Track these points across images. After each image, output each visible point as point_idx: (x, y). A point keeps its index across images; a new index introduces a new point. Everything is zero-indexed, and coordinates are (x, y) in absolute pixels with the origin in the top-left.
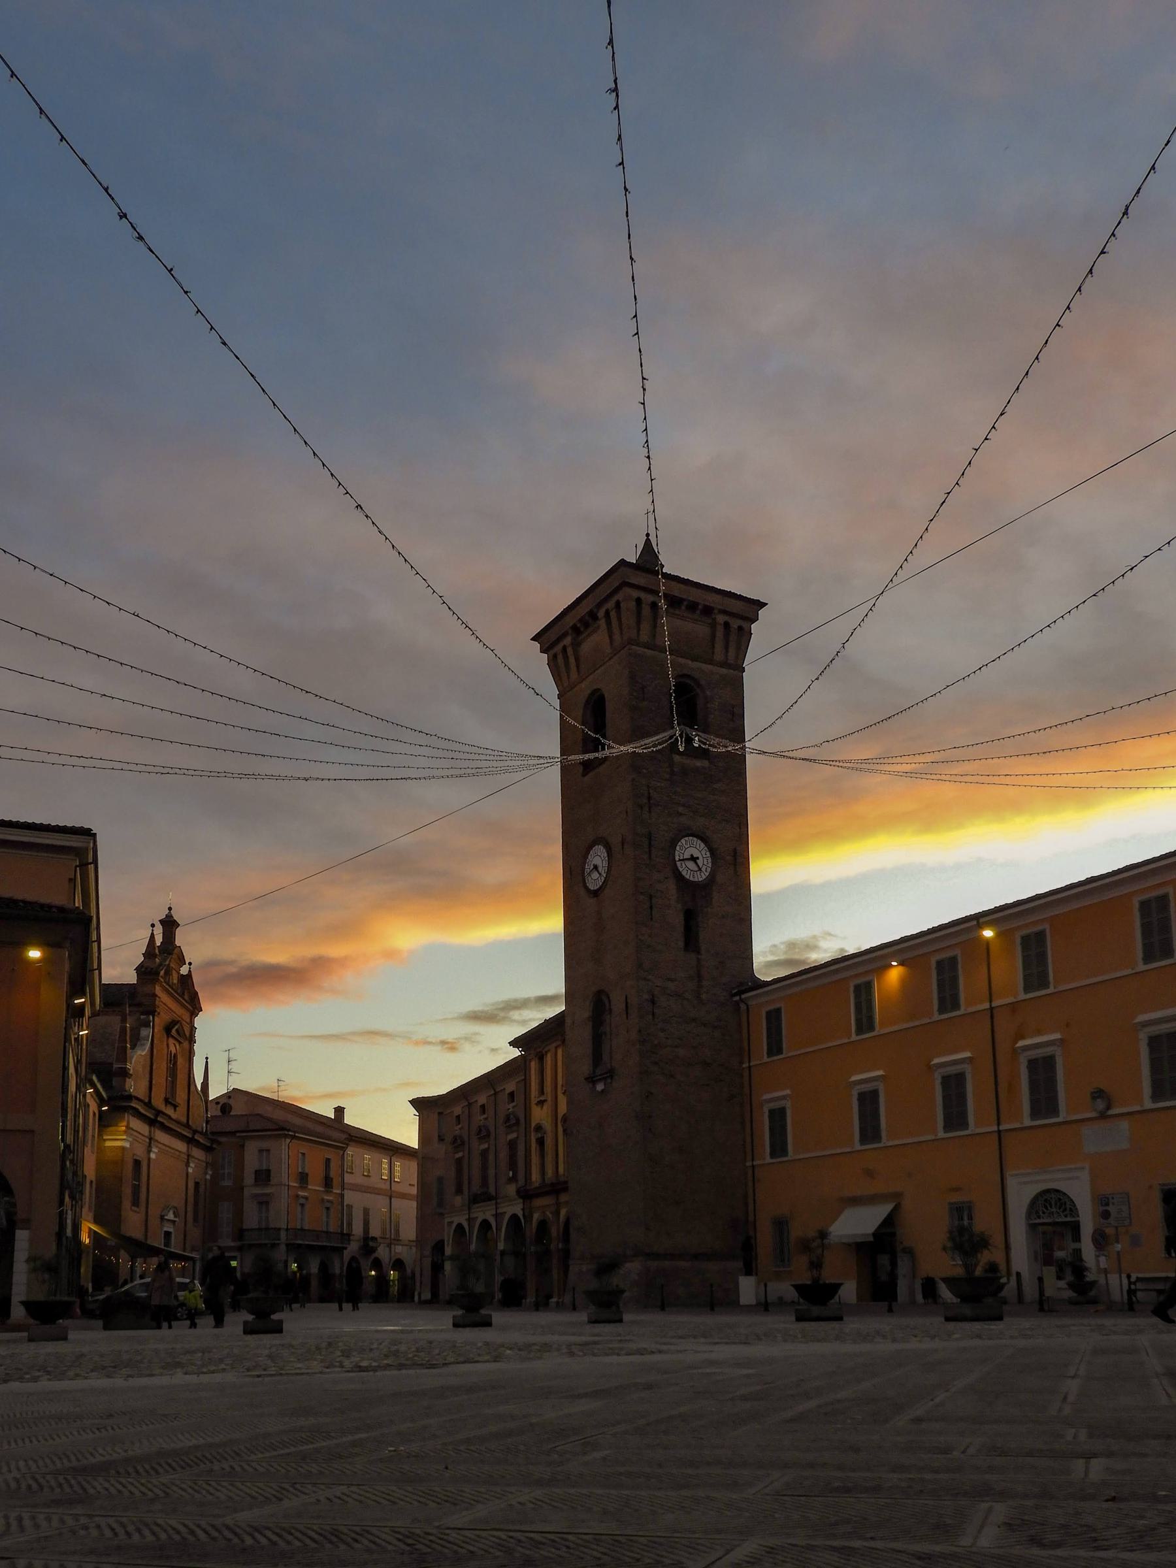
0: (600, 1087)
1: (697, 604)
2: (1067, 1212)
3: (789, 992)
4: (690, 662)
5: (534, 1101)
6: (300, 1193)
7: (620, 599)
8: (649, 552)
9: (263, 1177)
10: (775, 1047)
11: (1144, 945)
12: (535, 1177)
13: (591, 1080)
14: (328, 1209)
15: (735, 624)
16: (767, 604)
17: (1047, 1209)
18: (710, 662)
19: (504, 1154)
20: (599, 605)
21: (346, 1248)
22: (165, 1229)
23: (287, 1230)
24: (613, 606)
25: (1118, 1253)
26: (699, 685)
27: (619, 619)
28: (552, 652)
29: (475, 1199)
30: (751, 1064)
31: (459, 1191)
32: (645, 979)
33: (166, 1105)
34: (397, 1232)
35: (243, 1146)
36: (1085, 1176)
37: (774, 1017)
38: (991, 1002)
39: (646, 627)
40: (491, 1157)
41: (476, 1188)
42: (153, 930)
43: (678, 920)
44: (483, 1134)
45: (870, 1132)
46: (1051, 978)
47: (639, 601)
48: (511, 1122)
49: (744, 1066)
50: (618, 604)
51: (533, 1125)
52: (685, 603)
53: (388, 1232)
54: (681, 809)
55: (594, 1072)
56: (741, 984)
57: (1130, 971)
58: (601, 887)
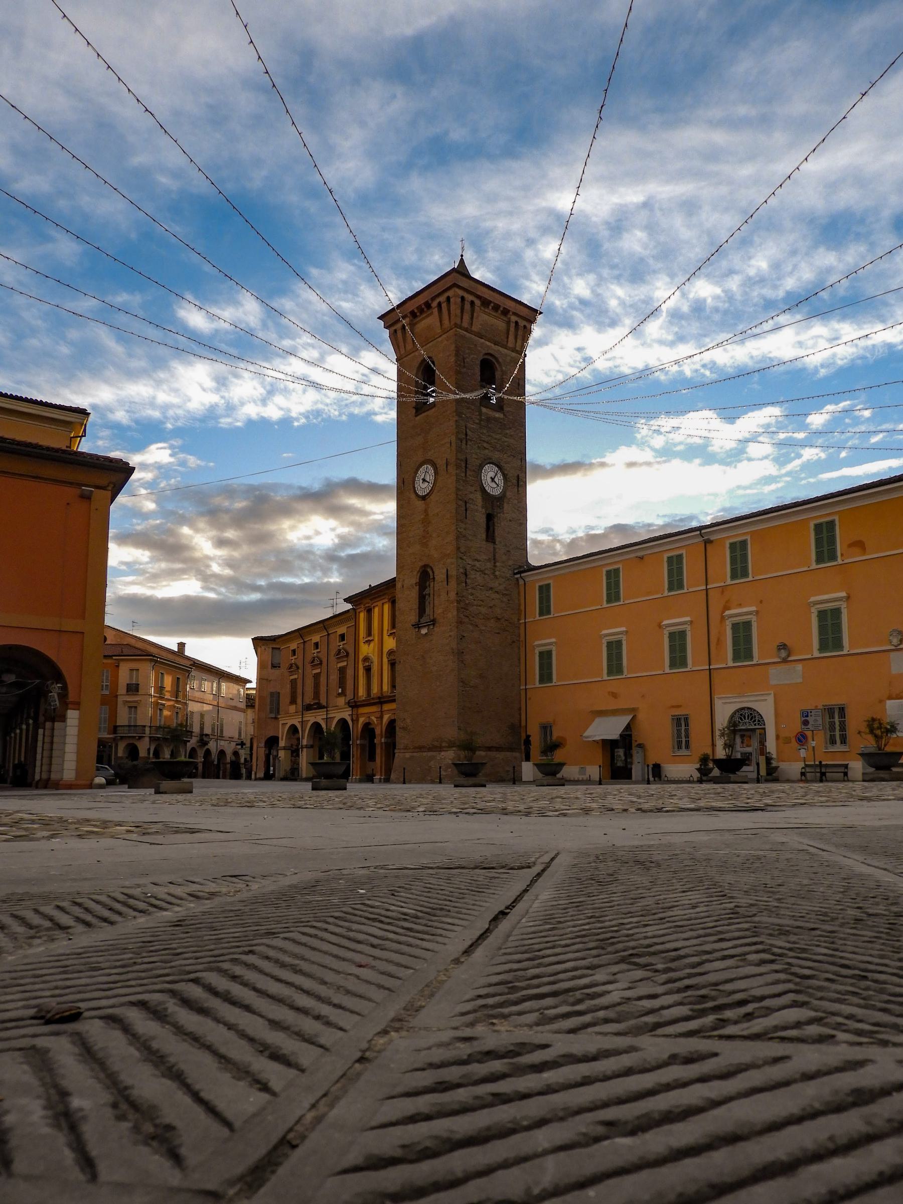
0: (424, 631)
2: (756, 722)
3: (556, 573)
4: (493, 345)
5: (362, 640)
7: (451, 296)
9: (133, 688)
10: (545, 609)
11: (817, 553)
12: (362, 692)
13: (417, 626)
14: (177, 713)
15: (522, 323)
17: (742, 720)
18: (505, 347)
19: (334, 677)
20: (433, 299)
21: (189, 741)
23: (150, 727)
24: (445, 300)
25: (814, 747)
27: (449, 310)
28: (393, 328)
29: (308, 708)
31: (293, 701)
32: (461, 558)
34: (222, 731)
35: (118, 666)
36: (771, 699)
37: (545, 590)
38: (707, 585)
39: (466, 317)
40: (323, 679)
41: (309, 699)
43: (482, 520)
44: (316, 662)
45: (615, 666)
46: (750, 571)
47: (463, 298)
48: (342, 655)
49: (521, 622)
50: (448, 299)
51: (361, 657)
52: (492, 305)
53: (216, 731)
54: (485, 445)
55: (419, 621)
56: (520, 567)
57: (806, 569)
58: (428, 494)
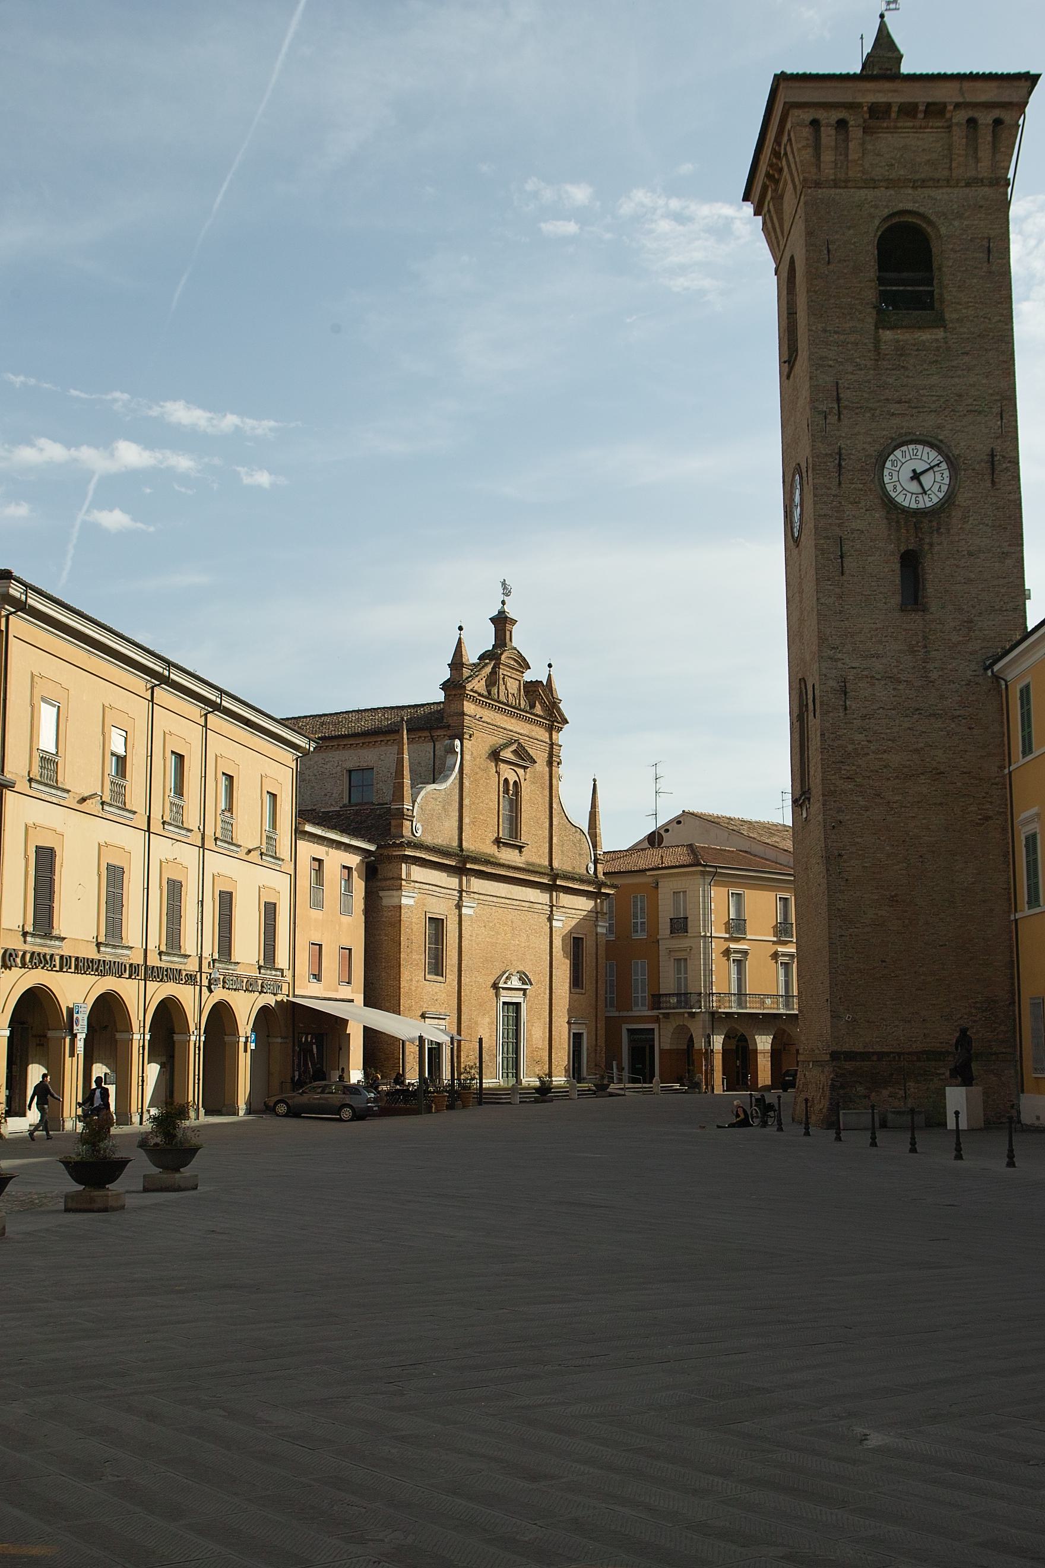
1: (915, 105)
6: (732, 946)
8: (884, 42)
16: (1040, 75)
22: (503, 999)
26: (930, 223)
30: (1011, 770)
33: (499, 847)
42: (460, 634)
